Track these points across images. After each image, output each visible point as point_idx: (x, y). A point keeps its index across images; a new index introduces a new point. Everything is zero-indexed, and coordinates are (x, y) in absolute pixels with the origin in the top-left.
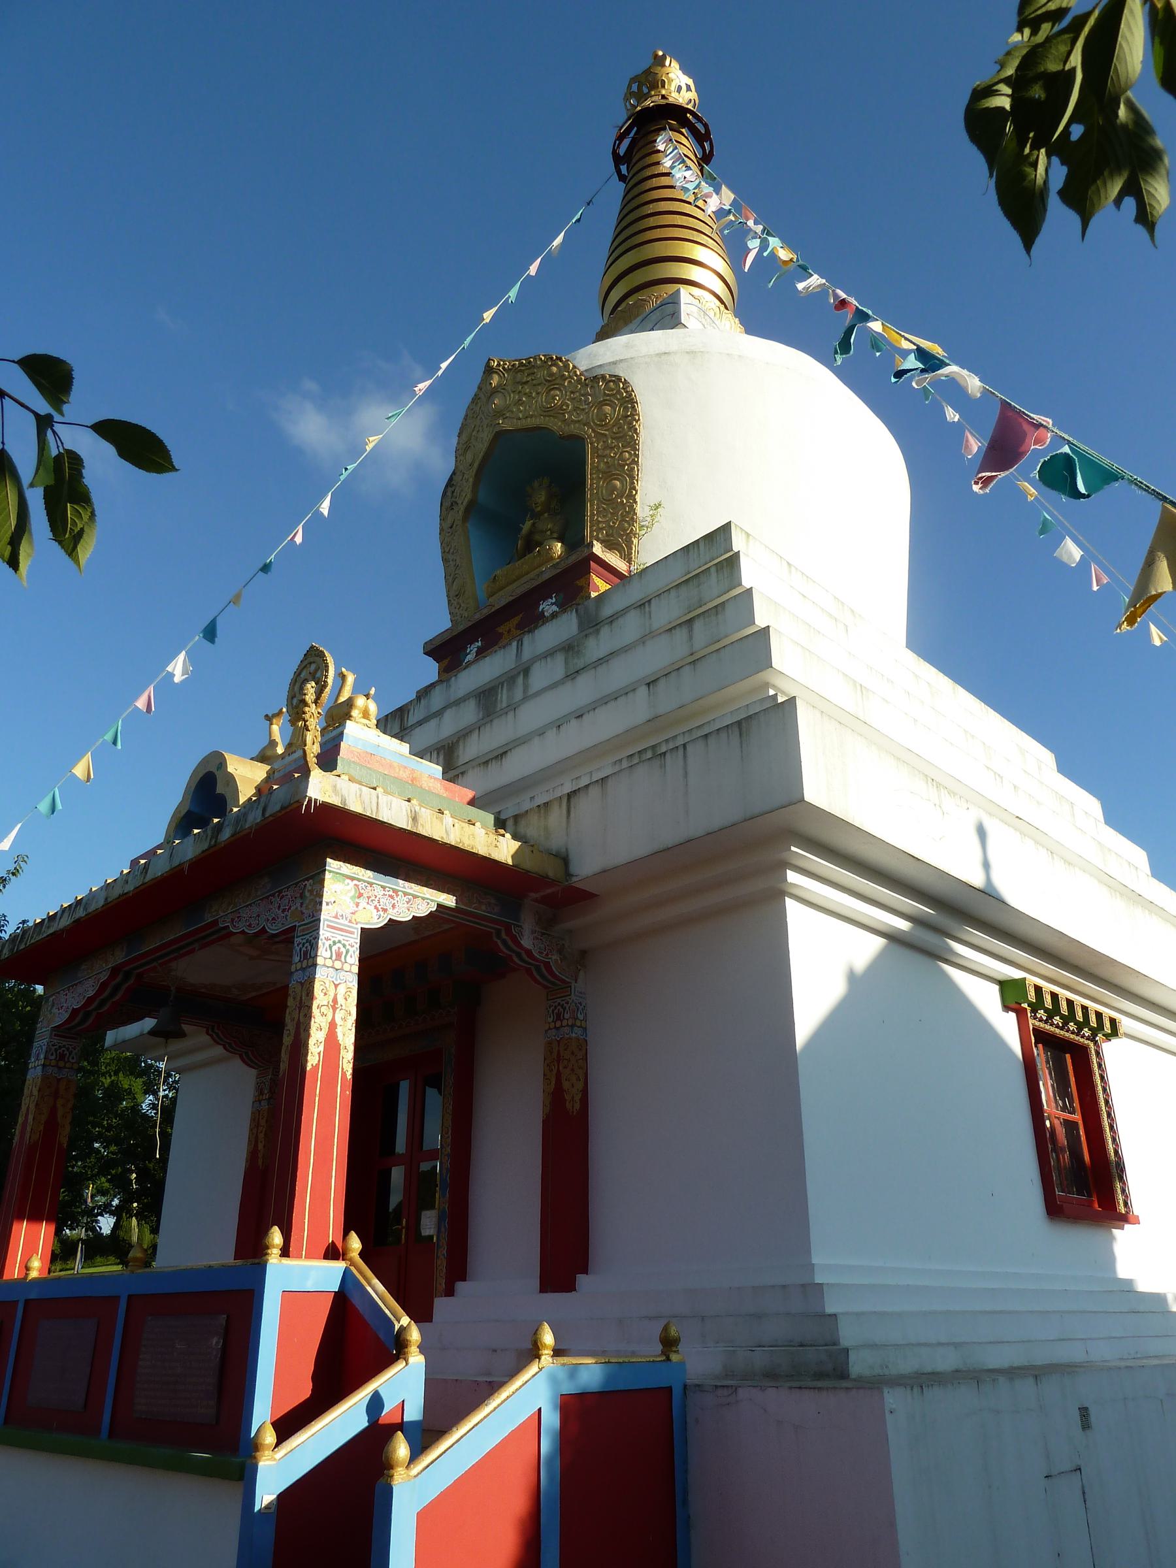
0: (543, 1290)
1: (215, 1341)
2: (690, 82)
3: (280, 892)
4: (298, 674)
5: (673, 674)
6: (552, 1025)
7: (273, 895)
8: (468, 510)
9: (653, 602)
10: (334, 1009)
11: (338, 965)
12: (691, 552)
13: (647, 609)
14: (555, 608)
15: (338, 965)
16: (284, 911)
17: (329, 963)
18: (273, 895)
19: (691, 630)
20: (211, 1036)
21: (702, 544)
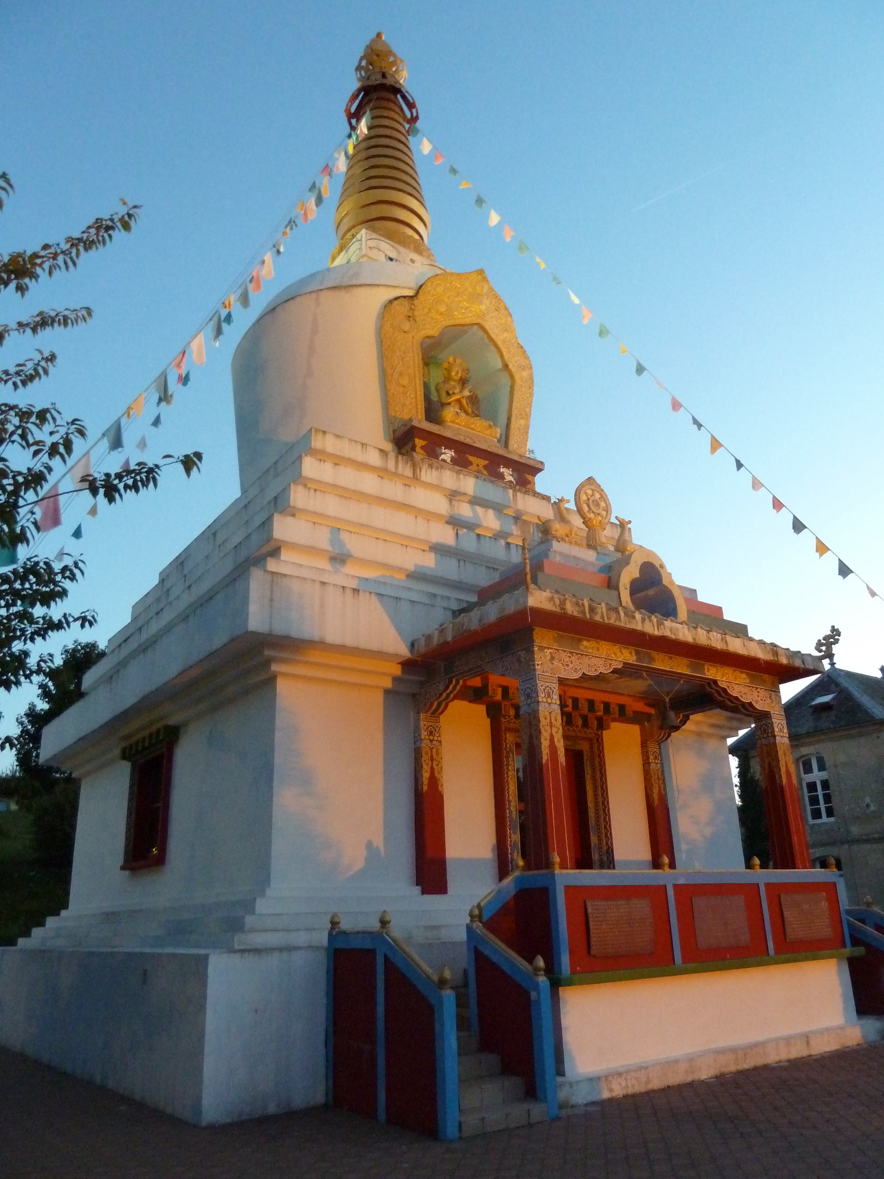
3: (757, 688)
16: (507, 669)
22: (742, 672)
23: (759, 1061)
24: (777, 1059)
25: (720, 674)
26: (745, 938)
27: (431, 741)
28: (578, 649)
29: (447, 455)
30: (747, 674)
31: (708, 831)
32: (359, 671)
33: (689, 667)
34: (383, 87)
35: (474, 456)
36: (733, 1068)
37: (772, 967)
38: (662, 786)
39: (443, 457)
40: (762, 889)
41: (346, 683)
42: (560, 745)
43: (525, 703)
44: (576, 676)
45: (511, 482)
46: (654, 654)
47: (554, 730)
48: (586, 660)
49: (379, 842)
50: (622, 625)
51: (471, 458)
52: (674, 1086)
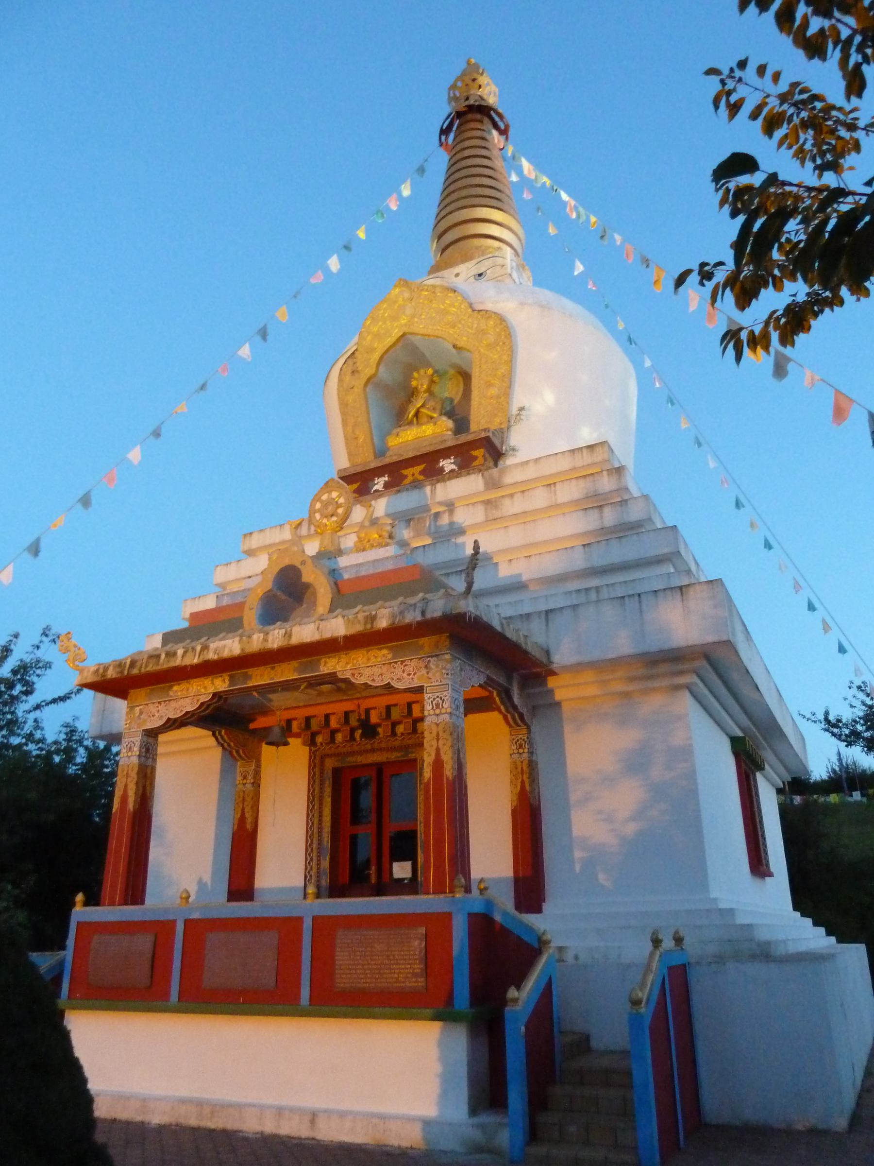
0: (469, 915)
1: (416, 943)
2: (497, 90)
3: (402, 662)
4: (313, 500)
5: (603, 543)
6: (516, 751)
7: (396, 663)
8: (368, 380)
9: (557, 485)
10: (438, 740)
11: (438, 711)
12: (576, 455)
13: (553, 488)
14: (454, 467)
15: (438, 711)
17: (432, 712)
18: (396, 663)
19: (601, 513)
20: (217, 739)
21: (585, 451)
22: (380, 649)
23: (231, 1125)
24: (258, 1128)
25: (342, 664)
26: (269, 980)
27: (244, 784)
28: (168, 696)
29: (448, 465)
30: (387, 648)
31: (631, 829)
32: (189, 739)
33: (295, 670)
34: (471, 108)
35: (407, 468)
36: (193, 1122)
37: (270, 1018)
38: (248, 814)
39: (447, 470)
40: (308, 924)
41: (198, 749)
42: (131, 793)
43: (432, 712)
44: (161, 723)
45: (452, 471)
46: (250, 671)
47: (129, 780)
48: (173, 704)
49: (207, 878)
50: (165, 666)
51: (405, 472)
52: (120, 1121)
